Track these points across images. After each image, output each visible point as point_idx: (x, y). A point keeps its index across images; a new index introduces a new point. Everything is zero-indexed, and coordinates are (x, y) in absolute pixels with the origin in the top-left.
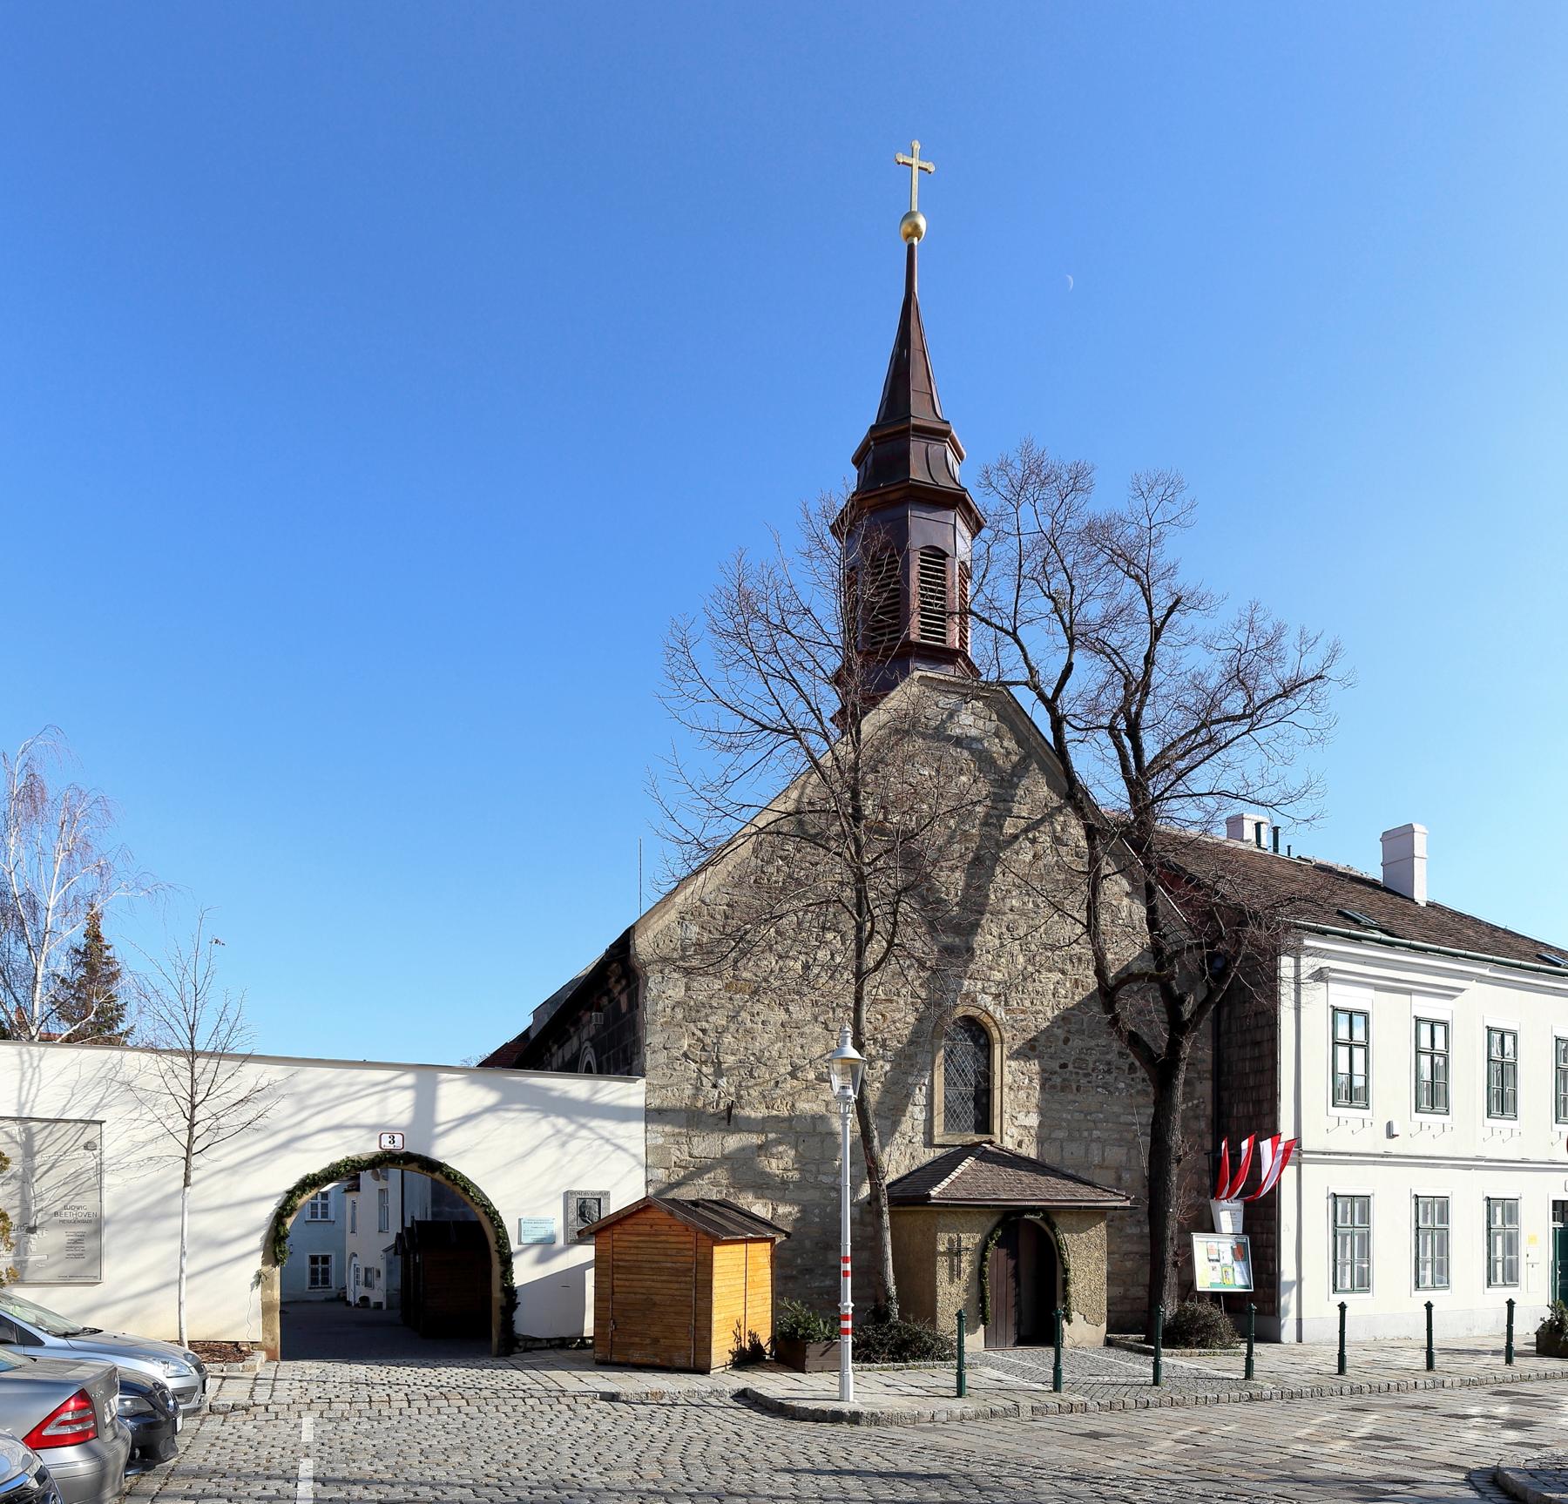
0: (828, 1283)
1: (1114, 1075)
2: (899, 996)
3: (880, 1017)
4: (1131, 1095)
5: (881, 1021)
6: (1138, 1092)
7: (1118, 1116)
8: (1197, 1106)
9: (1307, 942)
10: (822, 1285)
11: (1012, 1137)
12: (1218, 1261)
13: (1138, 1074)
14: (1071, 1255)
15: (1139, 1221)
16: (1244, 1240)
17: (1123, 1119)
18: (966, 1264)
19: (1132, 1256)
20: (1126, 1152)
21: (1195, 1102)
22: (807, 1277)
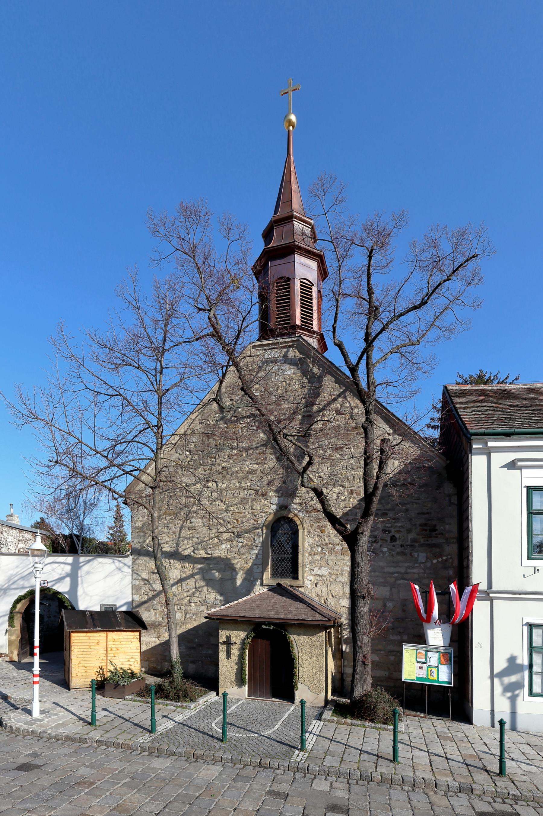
0: (210, 652)
1: (380, 543)
2: (245, 509)
3: (235, 521)
4: (392, 555)
5: (236, 523)
6: (398, 553)
7: (383, 568)
8: (446, 560)
9: (490, 444)
10: (208, 653)
11: (310, 581)
12: (425, 663)
13: (398, 542)
14: (300, 651)
15: (400, 632)
16: (450, 652)
17: (387, 570)
18: (235, 651)
19: (395, 653)
20: (389, 589)
21: (444, 558)
22: (200, 648)
